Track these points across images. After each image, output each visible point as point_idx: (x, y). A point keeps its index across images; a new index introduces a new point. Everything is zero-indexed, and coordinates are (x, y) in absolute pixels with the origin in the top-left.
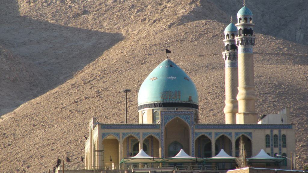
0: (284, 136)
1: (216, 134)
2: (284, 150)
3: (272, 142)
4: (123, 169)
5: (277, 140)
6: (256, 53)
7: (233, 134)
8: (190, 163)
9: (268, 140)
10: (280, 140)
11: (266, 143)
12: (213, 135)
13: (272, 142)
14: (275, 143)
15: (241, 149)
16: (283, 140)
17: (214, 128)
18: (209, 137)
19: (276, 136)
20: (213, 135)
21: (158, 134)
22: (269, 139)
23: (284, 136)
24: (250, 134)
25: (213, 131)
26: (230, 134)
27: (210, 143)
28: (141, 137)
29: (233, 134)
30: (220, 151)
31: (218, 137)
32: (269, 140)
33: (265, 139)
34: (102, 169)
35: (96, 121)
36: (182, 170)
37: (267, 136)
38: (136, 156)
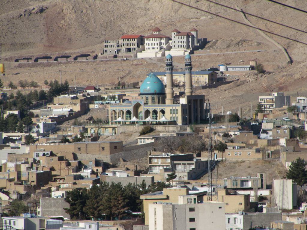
0: (177, 109)
2: (171, 115)
3: (172, 112)
4: (111, 217)
6: (97, 132)
11: (171, 112)
12: (151, 109)
13: (172, 112)
15: (240, 113)
17: (151, 106)
19: (174, 109)
20: (151, 109)
21: (131, 109)
23: (177, 109)
24: (165, 109)
26: (157, 109)
30: (11, 114)
34: (275, 103)
37: (171, 109)
38: (131, 111)
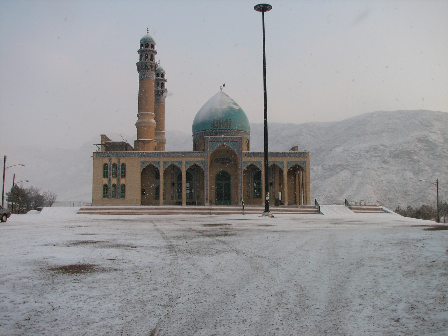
1: (165, 163)
5: (106, 194)
7: (184, 162)
8: (23, 326)
9: (106, 169)
10: (119, 169)
12: (162, 164)
14: (122, 172)
16: (122, 169)
18: (179, 166)
22: (107, 168)
23: (123, 186)
25: (183, 160)
27: (260, 173)
28: (285, 166)
29: (184, 162)
31: (166, 167)
32: (107, 170)
33: (160, 197)
35: (442, 155)
36: (217, 227)
